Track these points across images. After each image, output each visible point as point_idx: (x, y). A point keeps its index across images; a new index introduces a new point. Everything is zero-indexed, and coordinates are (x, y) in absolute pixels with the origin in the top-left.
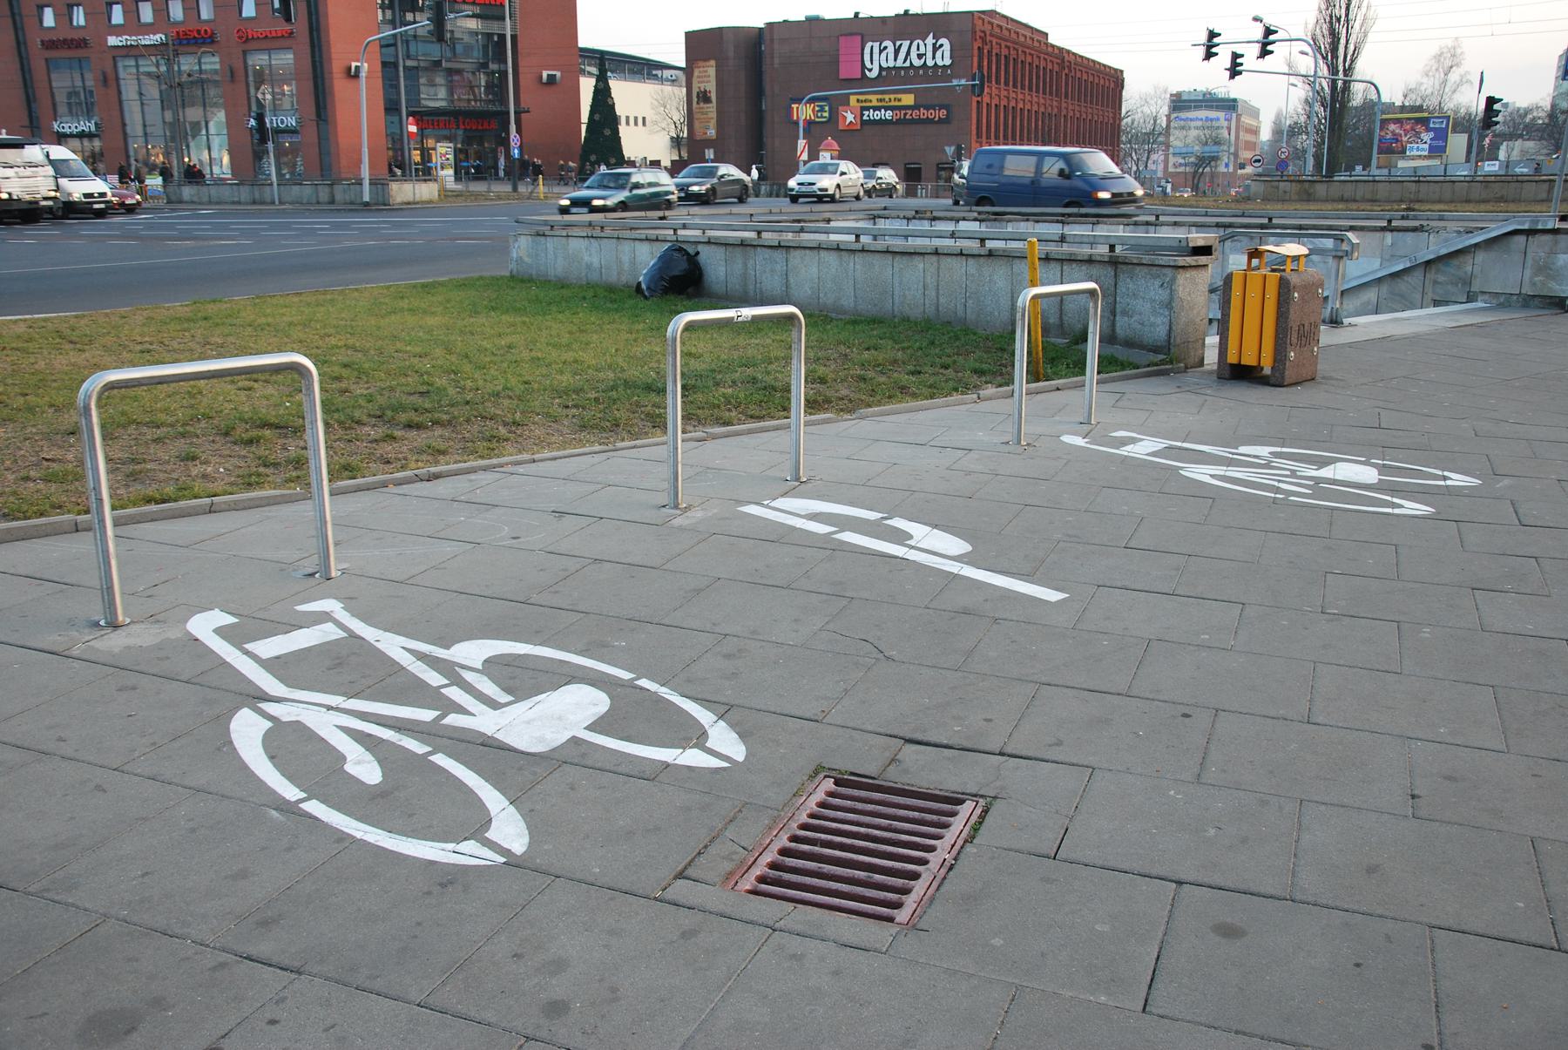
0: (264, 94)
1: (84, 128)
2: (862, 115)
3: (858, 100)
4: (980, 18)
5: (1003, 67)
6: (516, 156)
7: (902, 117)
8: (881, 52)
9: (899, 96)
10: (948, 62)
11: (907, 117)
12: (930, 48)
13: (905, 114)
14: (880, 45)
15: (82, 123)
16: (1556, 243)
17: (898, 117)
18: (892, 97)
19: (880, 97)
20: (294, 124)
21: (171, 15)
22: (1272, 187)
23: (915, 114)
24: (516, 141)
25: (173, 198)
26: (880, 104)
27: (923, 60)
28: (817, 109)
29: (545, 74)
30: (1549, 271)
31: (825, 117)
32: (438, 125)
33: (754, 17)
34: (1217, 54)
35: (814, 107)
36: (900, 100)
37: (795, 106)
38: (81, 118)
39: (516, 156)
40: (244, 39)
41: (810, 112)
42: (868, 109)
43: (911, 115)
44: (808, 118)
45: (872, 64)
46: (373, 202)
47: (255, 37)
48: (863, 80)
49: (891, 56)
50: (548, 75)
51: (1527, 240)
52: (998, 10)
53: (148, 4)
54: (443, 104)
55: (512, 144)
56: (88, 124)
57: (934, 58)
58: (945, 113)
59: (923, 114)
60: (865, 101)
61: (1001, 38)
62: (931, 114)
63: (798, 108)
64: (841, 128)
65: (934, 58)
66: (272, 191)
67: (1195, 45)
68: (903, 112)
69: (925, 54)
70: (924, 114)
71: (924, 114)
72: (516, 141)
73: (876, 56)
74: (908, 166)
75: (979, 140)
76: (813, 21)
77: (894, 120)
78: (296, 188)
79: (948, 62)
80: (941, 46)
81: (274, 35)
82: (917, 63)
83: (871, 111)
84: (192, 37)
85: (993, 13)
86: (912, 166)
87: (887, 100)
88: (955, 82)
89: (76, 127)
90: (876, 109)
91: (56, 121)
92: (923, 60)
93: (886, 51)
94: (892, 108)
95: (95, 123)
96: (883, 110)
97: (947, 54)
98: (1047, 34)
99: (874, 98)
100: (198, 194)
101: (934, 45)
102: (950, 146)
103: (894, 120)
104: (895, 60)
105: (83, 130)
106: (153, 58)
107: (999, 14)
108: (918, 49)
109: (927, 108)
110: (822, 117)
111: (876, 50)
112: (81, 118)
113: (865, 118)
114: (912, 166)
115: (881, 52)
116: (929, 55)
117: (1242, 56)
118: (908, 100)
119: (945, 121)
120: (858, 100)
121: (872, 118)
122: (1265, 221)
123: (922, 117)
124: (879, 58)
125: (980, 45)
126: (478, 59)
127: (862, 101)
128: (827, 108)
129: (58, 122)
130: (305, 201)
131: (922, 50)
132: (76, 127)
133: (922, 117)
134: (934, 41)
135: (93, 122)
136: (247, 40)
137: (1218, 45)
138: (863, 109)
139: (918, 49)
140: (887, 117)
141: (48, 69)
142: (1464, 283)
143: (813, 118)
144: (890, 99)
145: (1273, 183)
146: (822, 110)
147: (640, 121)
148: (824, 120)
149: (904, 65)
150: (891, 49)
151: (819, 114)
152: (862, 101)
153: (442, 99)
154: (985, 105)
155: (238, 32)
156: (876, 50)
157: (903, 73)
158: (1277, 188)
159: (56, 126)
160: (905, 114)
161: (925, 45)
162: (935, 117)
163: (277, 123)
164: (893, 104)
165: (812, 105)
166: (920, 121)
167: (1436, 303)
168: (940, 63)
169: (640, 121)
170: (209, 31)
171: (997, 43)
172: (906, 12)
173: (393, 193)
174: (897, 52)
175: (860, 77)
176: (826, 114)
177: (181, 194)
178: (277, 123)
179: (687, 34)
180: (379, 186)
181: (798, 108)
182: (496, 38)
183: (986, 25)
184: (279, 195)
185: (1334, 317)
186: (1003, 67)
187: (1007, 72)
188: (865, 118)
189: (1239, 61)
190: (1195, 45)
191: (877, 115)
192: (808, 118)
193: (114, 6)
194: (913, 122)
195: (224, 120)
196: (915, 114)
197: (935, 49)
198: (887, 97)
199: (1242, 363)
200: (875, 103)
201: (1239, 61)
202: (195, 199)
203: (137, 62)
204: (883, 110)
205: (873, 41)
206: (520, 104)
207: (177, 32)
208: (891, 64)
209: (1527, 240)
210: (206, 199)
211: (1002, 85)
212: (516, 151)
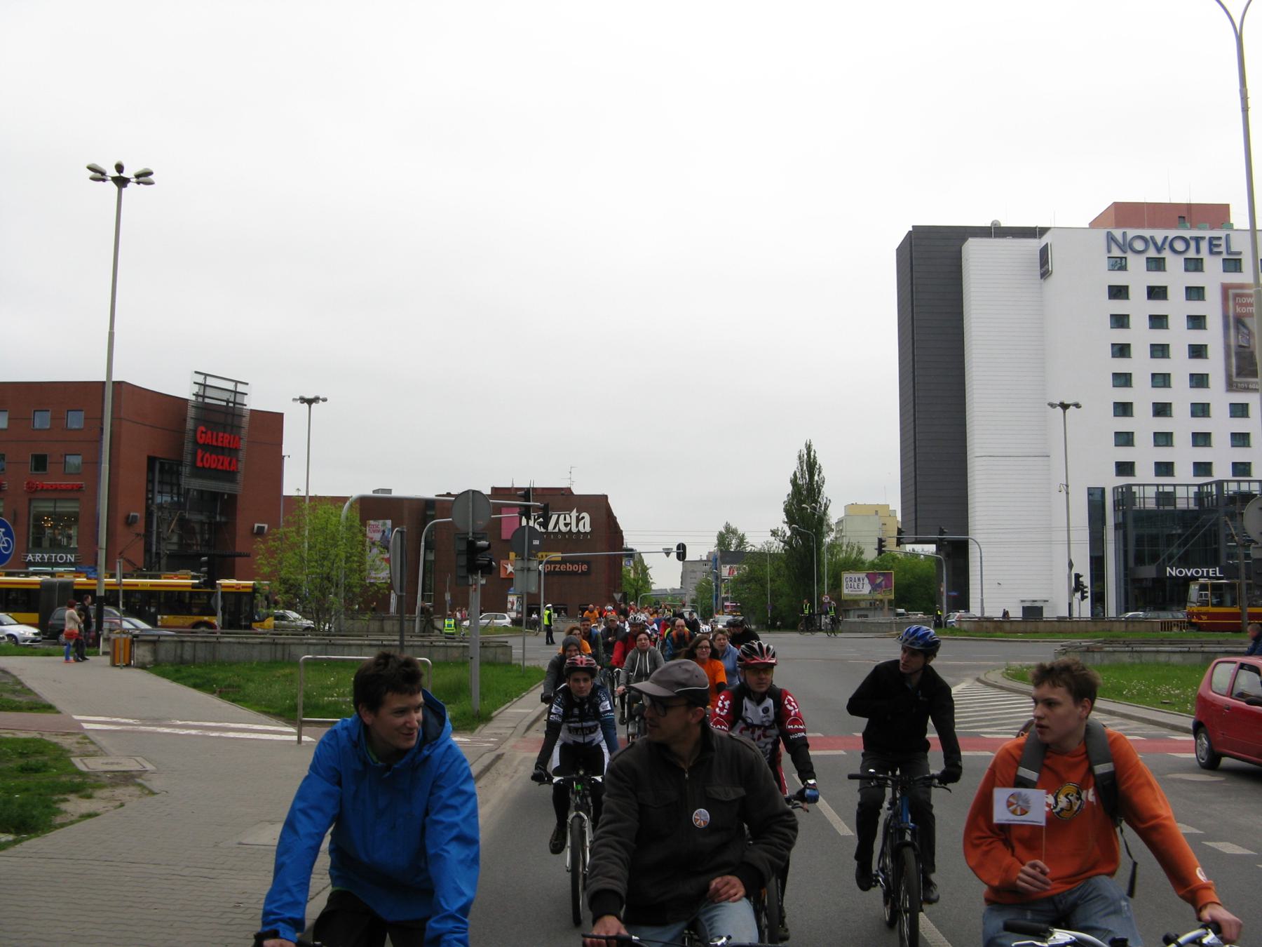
10: (588, 529)
11: (557, 569)
13: (555, 568)
20: (73, 560)
23: (563, 567)
27: (569, 527)
29: (256, 525)
43: (560, 568)
57: (577, 526)
65: (577, 526)
68: (553, 566)
69: (570, 524)
79: (588, 529)
80: (583, 518)
82: (564, 529)
92: (569, 527)
93: (583, 521)
101: (577, 517)
102: (618, 593)
108: (565, 519)
117: (1081, 576)
123: (568, 569)
131: (568, 521)
134: (577, 514)
139: (565, 519)
153: (174, 543)
157: (552, 536)
161: (571, 517)
162: (67, 559)
168: (582, 530)
182: (226, 497)
189: (883, 544)
194: (561, 573)
196: (563, 567)
197: (578, 520)
201: (883, 544)
203: (55, 503)
206: (146, 543)
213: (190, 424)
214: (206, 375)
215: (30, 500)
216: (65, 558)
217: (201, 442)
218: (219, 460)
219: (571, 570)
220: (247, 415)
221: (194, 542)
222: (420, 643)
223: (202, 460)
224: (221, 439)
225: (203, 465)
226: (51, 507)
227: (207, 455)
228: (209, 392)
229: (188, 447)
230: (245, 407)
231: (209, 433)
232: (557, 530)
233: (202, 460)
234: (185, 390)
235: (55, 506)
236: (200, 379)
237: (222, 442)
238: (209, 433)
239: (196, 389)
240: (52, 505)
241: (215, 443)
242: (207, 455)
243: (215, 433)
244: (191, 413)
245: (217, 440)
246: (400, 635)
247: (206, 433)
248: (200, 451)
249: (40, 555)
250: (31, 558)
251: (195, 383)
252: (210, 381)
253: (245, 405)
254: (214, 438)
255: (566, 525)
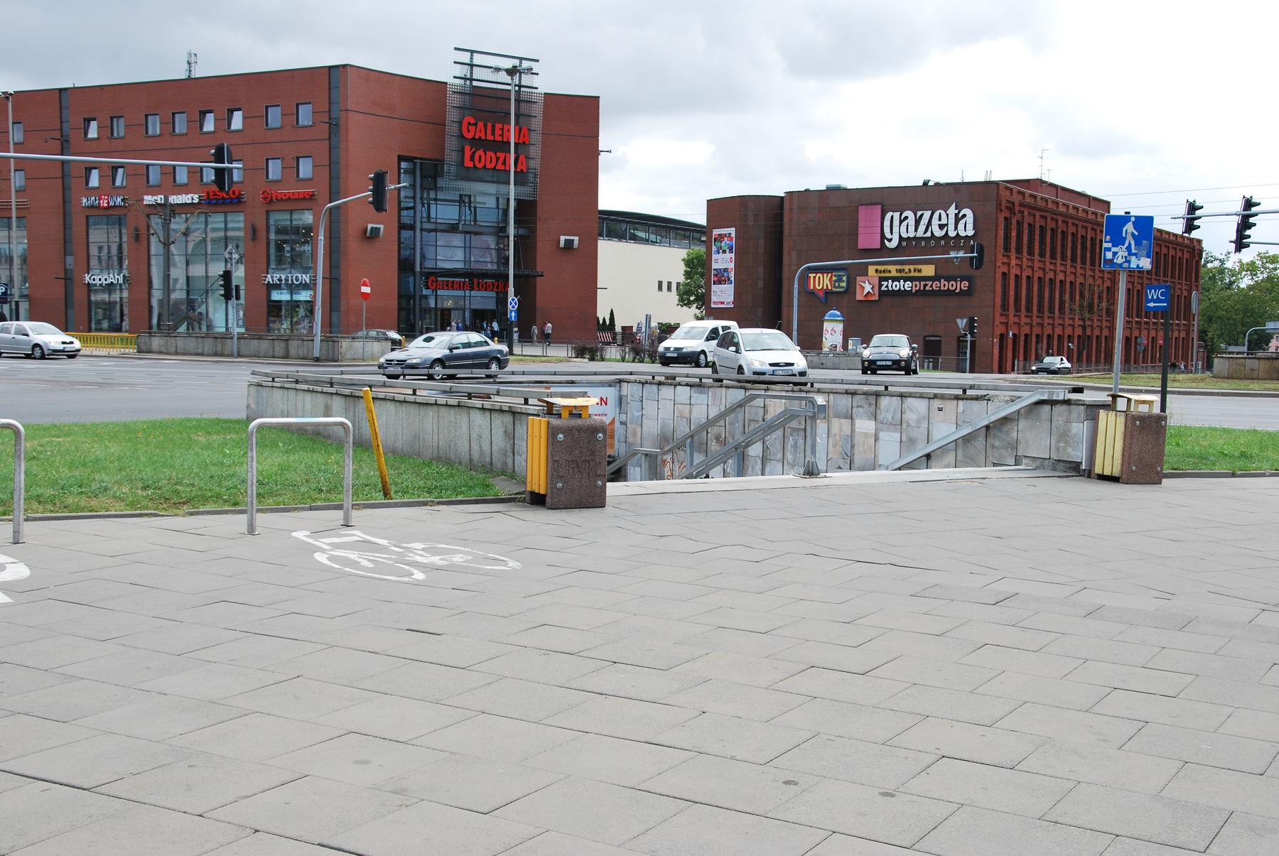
0: (231, 253)
1: (113, 281)
2: (880, 286)
3: (877, 271)
4: (1007, 188)
5: (1037, 238)
6: (513, 319)
7: (922, 288)
8: (901, 222)
9: (919, 267)
10: (970, 232)
11: (927, 288)
12: (952, 221)
13: (925, 286)
14: (901, 215)
15: (111, 275)
16: (1070, 412)
17: (918, 288)
18: (912, 267)
19: (899, 267)
20: (308, 282)
21: (177, 178)
22: (1239, 365)
23: (936, 285)
24: (513, 303)
25: (143, 348)
26: (899, 275)
28: (834, 278)
30: (1066, 438)
31: (843, 287)
32: (452, 287)
33: (776, 187)
34: (1199, 227)
35: (831, 277)
36: (920, 271)
37: (812, 275)
38: (111, 271)
39: (513, 319)
40: (268, 200)
41: (827, 281)
42: (886, 279)
43: (931, 286)
44: (825, 288)
45: (892, 234)
46: (323, 357)
47: (279, 198)
48: (882, 250)
49: (912, 228)
50: (566, 240)
51: (1052, 409)
52: (1045, 178)
53: (561, 246)
54: (460, 266)
55: (510, 307)
56: (117, 277)
57: (956, 228)
58: (967, 285)
59: (944, 285)
60: (884, 271)
61: (1034, 208)
62: (952, 285)
63: (814, 277)
64: (859, 298)
65: (956, 228)
66: (232, 343)
67: (1175, 218)
68: (923, 283)
69: (947, 225)
70: (944, 285)
71: (944, 285)
72: (513, 303)
73: (896, 229)
74: (927, 338)
75: (1006, 313)
76: (834, 191)
77: (914, 291)
78: (255, 342)
79: (970, 232)
80: (964, 216)
81: (296, 197)
82: (939, 233)
83: (890, 281)
84: (221, 197)
85: (1039, 183)
86: (932, 338)
87: (907, 270)
88: (953, 254)
89: (106, 279)
90: (895, 279)
91: (88, 273)
93: (963, 222)
94: (912, 279)
95: (124, 276)
96: (902, 281)
97: (970, 226)
98: (1108, 203)
99: (893, 268)
100: (166, 345)
101: (956, 215)
102: (962, 318)
103: (914, 291)
104: (916, 230)
105: (112, 282)
106: (184, 216)
107: (1046, 182)
108: (940, 220)
109: (948, 279)
110: (839, 287)
111: (896, 223)
112: (111, 271)
113: (883, 288)
114: (932, 338)
115: (901, 222)
116: (951, 227)
118: (929, 270)
119: (967, 293)
120: (877, 271)
121: (890, 289)
122: (960, 392)
123: (942, 288)
124: (899, 228)
125: (1008, 216)
126: (498, 223)
127: (880, 272)
128: (844, 278)
129: (90, 275)
130: (262, 354)
131: (944, 221)
132: (106, 279)
133: (942, 288)
134: (957, 211)
135: (121, 275)
136: (271, 202)
137: (1200, 218)
138: (881, 279)
139: (940, 220)
140: (934, 288)
141: (88, 226)
142: (1012, 448)
143: (830, 288)
144: (910, 270)
145: (1238, 361)
146: (840, 280)
147: (665, 286)
148: (841, 290)
149: (925, 236)
150: (911, 221)
151: (837, 284)
152: (880, 272)
154: (1012, 277)
155: (263, 193)
156: (896, 223)
157: (923, 243)
158: (1244, 366)
159: (87, 278)
160: (925, 286)
161: (947, 215)
162: (956, 289)
163: (292, 280)
164: (913, 274)
165: (830, 275)
166: (940, 293)
167: (995, 465)
168: (962, 234)
169: (665, 286)
170: (237, 193)
171: (1041, 216)
172: (925, 184)
173: (342, 350)
174: (917, 222)
175: (879, 247)
176: (844, 284)
177: (150, 345)
178: (292, 280)
179: (710, 203)
180: (330, 343)
181: (814, 277)
183: (1015, 195)
184: (238, 348)
185: (811, 470)
186: (1037, 238)
187: (1042, 242)
188: (883, 288)
190: (1175, 218)
191: (896, 286)
192: (825, 288)
193: (93, 171)
194: (933, 293)
195: (243, 275)
196: (936, 285)
197: (957, 220)
198: (906, 268)
199: (1105, 474)
200: (894, 274)
202: (163, 349)
203: (226, 217)
204: (902, 281)
205: (893, 212)
207: (208, 193)
208: (911, 235)
209: (1052, 409)
210: (173, 350)
211: (1037, 257)
212: (513, 314)
213: (452, 116)
214: (472, 52)
215: (268, 212)
216: (300, 278)
217: (470, 136)
218: (498, 159)
219: (946, 288)
220: (541, 101)
221: (488, 260)
222: (553, 390)
223: (472, 159)
224: (500, 132)
225: (474, 165)
226: (220, 222)
227: (480, 152)
228: (478, 74)
229: (451, 143)
230: (534, 91)
231: (480, 124)
232: (928, 234)
233: (472, 159)
234: (445, 71)
235: (226, 222)
236: (465, 57)
237: (502, 135)
238: (480, 124)
239: (462, 71)
240: (288, 217)
241: (490, 137)
242: (480, 152)
243: (489, 125)
244: (452, 100)
245: (493, 134)
246: (1162, 374)
247: (476, 124)
248: (467, 148)
249: (278, 276)
250: (270, 280)
251: (455, 62)
252: (478, 59)
253: (537, 88)
254: (489, 132)
255: (941, 227)
